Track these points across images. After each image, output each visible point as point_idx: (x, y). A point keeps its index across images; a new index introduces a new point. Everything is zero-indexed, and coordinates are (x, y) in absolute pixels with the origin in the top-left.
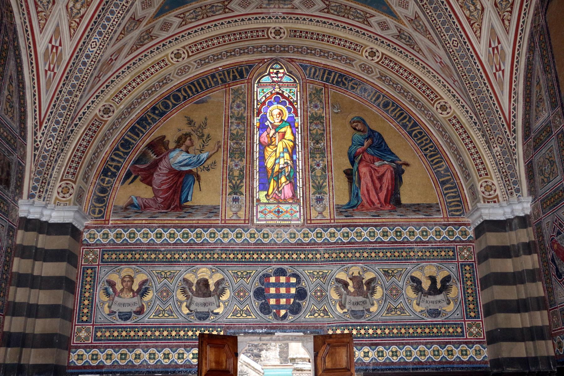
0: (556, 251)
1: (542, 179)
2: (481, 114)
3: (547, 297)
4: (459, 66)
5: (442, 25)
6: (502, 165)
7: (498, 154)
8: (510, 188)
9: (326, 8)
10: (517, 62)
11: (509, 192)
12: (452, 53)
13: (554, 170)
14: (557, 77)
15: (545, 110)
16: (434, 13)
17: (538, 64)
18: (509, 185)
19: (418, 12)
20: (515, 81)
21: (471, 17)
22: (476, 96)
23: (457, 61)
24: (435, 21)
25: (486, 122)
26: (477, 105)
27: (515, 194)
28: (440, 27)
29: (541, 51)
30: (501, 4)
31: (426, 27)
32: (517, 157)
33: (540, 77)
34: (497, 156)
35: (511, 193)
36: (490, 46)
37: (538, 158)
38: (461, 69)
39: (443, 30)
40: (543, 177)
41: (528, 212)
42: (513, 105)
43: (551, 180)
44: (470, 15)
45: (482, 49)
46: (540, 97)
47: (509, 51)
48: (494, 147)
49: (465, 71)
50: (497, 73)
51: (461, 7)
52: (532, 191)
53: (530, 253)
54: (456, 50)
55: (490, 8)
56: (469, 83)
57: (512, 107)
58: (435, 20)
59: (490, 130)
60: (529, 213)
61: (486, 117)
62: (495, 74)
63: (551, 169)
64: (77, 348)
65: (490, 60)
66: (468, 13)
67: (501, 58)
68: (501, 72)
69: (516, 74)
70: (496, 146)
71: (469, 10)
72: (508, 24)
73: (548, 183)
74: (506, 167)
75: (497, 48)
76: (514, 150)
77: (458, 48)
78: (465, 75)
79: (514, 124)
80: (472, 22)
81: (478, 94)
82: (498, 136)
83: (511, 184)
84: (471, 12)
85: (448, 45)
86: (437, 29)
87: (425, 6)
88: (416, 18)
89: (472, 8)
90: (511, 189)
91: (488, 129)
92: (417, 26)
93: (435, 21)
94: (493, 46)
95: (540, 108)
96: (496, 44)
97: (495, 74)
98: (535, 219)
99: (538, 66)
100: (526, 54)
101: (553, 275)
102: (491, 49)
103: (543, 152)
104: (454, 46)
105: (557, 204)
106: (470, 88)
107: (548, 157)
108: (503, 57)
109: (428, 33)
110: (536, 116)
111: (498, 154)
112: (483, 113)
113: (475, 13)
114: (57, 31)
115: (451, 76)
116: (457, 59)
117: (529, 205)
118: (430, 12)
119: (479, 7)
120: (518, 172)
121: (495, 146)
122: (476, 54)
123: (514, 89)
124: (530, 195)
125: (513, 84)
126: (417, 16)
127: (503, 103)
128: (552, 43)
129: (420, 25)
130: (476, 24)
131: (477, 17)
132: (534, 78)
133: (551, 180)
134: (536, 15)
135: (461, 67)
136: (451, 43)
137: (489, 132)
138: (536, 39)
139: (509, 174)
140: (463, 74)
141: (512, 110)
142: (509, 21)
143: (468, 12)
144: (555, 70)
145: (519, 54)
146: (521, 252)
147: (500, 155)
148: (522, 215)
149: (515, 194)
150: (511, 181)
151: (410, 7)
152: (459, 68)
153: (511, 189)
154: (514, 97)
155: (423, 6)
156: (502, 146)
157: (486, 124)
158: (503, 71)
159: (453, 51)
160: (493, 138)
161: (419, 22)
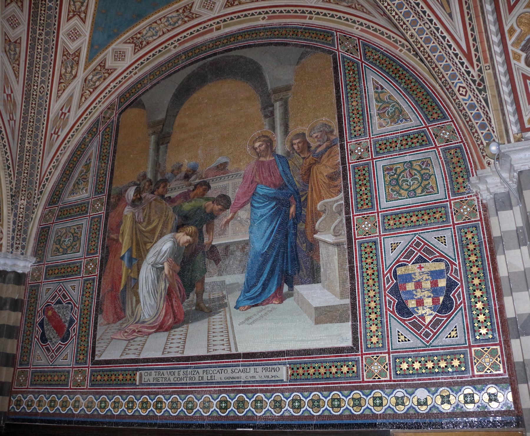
0: (49, 318)
1: (57, 248)
2: (25, 164)
3: (19, 356)
4: (33, 111)
5: (42, 68)
6: (21, 219)
7: (22, 207)
8: (18, 242)
9: (79, 16)
10: (72, 136)
11: (15, 246)
12: (34, 96)
13: (75, 245)
14: (112, 170)
15: (86, 190)
16: (43, 52)
17: (94, 148)
18: (18, 239)
19: (23, 38)
20: (62, 150)
21: (63, 76)
22: (31, 146)
23: (34, 105)
24: (38, 60)
25: (27, 173)
26: (28, 154)
27: (20, 249)
28: (39, 68)
29: (102, 140)
30: (89, 82)
31: (19, 56)
32: (34, 217)
33: (92, 160)
34: (20, 208)
35: (17, 248)
36: (61, 110)
37: (58, 227)
38: (33, 114)
39: (40, 73)
40: (58, 246)
41: (27, 271)
42: (51, 169)
43: (68, 252)
44: (64, 74)
45: (55, 107)
46: (84, 177)
47: (71, 122)
48: (21, 199)
49: (35, 118)
50: (54, 135)
51: (62, 63)
52: (36, 253)
53: (14, 310)
54: (39, 96)
55: (80, 80)
56: (32, 131)
57: (49, 170)
58: (40, 59)
59: (26, 182)
60: (26, 273)
61: (29, 169)
62: (52, 134)
63: (72, 243)
64: (17, 393)
65: (55, 121)
66: (63, 71)
67: (63, 124)
68: (56, 136)
69: (66, 144)
70: (24, 200)
71: (66, 70)
72: (83, 101)
73: (63, 254)
74: (23, 222)
75: (65, 114)
76: (34, 209)
77: (41, 95)
78: (33, 122)
79: (44, 186)
80: (61, 81)
81: (33, 145)
82: (30, 191)
83: (21, 239)
84: (66, 72)
85: (35, 87)
86: (36, 67)
87: (40, 41)
88: (16, 42)
89: (69, 70)
90: (19, 244)
91: (25, 180)
92: (10, 49)
93: (38, 60)
94: (63, 111)
95: (81, 187)
96: (66, 111)
97: (52, 134)
98: (31, 280)
99: (94, 149)
100: (83, 134)
101: (35, 337)
102: (61, 112)
103: (69, 225)
104: (40, 92)
105: (67, 276)
106: (30, 135)
107: (73, 232)
108: (65, 125)
109: (17, 62)
110: (73, 190)
111: (22, 207)
112: (28, 164)
113: (68, 75)
114: (70, 98)
115: (11, 113)
116: (35, 104)
117: (30, 265)
118: (41, 49)
119: (74, 72)
120: (30, 230)
121: (23, 198)
122: (49, 109)
123: (58, 156)
124: (35, 256)
125: (59, 152)
126: (18, 41)
127: (45, 163)
128: (119, 141)
129: (15, 50)
130: (63, 85)
131: (67, 79)
132: (84, 157)
133: (68, 252)
134: (109, 109)
135: (34, 113)
136: (39, 87)
137: (25, 183)
138: (102, 128)
139: (23, 229)
140: (32, 120)
141: (47, 173)
142: (86, 99)
143: (64, 70)
144: (113, 164)
145: (77, 130)
146: (8, 307)
147: (23, 208)
148: (20, 271)
149: (20, 249)
150: (22, 237)
151: (16, 30)
152: (31, 113)
153: (19, 244)
154: (54, 163)
155: (39, 39)
156: (29, 201)
157: (26, 175)
158: (58, 136)
159: (36, 95)
160: (25, 191)
161: (15, 48)
